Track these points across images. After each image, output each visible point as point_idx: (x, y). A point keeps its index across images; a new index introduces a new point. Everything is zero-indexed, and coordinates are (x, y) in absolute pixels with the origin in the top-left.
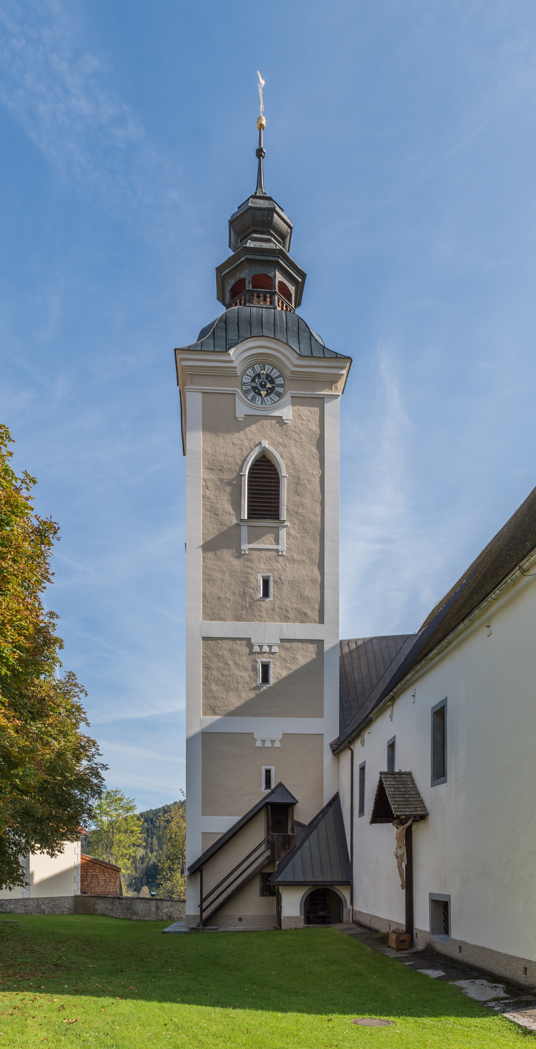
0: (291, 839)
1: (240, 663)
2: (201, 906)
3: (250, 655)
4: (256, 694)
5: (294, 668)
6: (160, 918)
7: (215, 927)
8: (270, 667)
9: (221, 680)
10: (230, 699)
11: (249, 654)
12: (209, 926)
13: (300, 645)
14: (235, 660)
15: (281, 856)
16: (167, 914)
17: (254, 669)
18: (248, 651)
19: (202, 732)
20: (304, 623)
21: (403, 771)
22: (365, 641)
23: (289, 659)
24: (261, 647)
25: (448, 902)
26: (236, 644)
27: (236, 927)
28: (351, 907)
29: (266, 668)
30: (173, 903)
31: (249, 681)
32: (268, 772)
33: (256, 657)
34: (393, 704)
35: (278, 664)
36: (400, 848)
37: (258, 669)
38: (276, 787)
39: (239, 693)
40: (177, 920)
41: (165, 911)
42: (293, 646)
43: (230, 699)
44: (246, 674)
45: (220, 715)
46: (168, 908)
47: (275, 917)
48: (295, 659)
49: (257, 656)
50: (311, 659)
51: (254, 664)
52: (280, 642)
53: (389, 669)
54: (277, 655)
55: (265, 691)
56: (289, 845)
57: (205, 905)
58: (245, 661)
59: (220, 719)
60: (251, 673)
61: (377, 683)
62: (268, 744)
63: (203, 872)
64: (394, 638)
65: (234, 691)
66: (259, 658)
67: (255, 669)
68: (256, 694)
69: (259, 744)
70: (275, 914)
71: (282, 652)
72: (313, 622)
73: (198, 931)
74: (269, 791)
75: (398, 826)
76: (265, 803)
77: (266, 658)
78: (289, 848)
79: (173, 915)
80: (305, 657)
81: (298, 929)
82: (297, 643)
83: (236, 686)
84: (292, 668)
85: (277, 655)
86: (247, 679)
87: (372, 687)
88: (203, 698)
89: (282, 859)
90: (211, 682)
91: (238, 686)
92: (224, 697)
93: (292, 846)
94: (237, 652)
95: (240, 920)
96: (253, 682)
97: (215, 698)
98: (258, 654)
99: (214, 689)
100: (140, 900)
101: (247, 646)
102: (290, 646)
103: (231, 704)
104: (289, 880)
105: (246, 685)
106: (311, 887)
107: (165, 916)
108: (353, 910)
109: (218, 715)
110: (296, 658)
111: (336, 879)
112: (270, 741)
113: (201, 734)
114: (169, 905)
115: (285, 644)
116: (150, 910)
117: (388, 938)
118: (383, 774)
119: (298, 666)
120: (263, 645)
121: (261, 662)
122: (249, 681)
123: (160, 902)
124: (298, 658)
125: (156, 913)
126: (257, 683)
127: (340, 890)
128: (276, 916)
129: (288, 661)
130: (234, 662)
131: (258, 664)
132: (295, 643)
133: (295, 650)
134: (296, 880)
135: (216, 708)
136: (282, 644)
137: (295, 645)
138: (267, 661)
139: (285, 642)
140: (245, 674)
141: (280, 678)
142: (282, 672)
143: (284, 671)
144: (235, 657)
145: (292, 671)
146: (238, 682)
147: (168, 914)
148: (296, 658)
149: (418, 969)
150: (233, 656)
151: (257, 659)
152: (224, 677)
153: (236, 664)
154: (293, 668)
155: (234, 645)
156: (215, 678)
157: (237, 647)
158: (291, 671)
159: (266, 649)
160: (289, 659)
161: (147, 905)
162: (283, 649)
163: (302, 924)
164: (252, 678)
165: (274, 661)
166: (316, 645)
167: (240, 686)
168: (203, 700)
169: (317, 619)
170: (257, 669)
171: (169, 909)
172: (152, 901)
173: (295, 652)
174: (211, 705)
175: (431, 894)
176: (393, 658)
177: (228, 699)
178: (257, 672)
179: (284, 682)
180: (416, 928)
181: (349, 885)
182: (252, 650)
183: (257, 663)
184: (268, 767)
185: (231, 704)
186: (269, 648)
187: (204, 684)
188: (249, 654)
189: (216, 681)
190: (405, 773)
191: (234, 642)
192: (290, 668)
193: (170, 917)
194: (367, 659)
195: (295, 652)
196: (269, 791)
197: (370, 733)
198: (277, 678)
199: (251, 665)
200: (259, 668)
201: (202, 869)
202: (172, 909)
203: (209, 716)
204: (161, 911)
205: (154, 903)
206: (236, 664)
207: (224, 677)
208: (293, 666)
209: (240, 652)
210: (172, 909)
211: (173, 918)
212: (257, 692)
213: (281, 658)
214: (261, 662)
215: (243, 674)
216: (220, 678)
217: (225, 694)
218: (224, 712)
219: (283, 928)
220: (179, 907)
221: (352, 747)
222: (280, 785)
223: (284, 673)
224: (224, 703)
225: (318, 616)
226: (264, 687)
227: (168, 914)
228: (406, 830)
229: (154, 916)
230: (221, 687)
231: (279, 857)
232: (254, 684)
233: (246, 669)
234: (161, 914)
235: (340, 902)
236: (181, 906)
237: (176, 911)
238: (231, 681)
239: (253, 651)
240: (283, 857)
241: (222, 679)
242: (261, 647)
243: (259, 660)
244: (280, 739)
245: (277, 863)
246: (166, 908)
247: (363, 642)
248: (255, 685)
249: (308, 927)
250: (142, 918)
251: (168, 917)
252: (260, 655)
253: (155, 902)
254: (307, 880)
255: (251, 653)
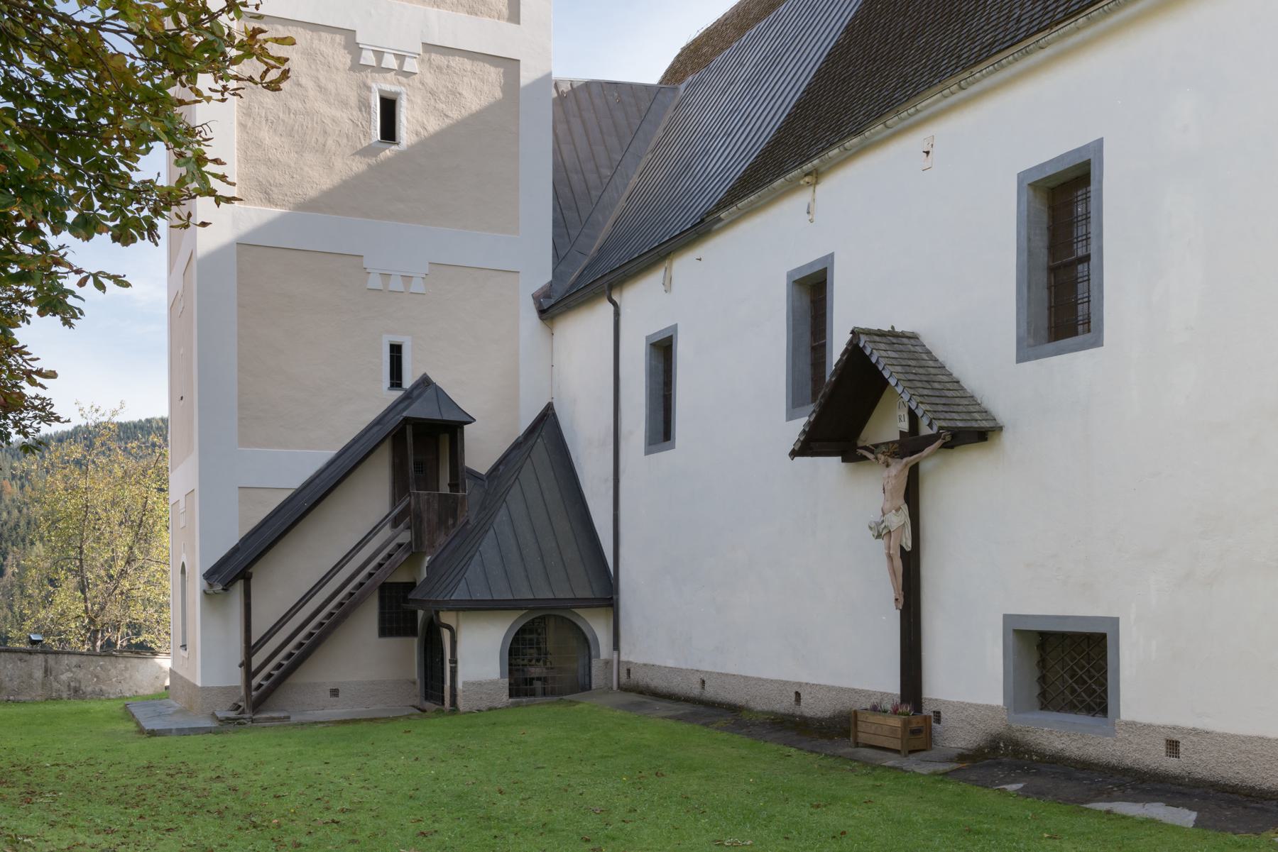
0: (459, 505)
1: (331, 86)
2: (246, 664)
3: (354, 72)
4: (369, 165)
5: (455, 115)
6: (54, 694)
7: (282, 715)
8: (401, 106)
9: (283, 121)
10: (306, 169)
11: (350, 69)
12: (272, 710)
13: (467, 64)
14: (318, 79)
15: (437, 544)
16: (69, 686)
17: (364, 105)
18: (348, 60)
19: (237, 243)
20: (476, 14)
21: (898, 329)
22: (575, 86)
23: (442, 92)
24: (379, 54)
25: (1104, 636)
26: (320, 40)
27: (326, 711)
28: (615, 656)
29: (389, 107)
30: (84, 658)
31: (350, 131)
32: (396, 350)
33: (367, 77)
34: (817, 183)
35: (419, 101)
36: (897, 510)
37: (373, 106)
38: (416, 386)
39: (328, 158)
40: (92, 698)
41: (64, 677)
42: (452, 64)
43: (306, 169)
44: (344, 115)
45: (282, 206)
46: (72, 672)
47: (414, 683)
48: (455, 94)
49: (369, 76)
50: (492, 100)
51: (365, 93)
52: (424, 52)
53: (631, 149)
54: (416, 81)
55: (389, 161)
56: (455, 518)
57: (256, 661)
58: (343, 83)
59: (283, 216)
60: (356, 113)
61: (612, 176)
62: (396, 284)
63: (253, 581)
64: (632, 87)
65: (317, 151)
66: (374, 80)
67: (364, 105)
68: (369, 165)
69: (375, 282)
70: (416, 677)
71: (429, 75)
72: (496, 15)
73: (239, 724)
74: (397, 394)
75: (890, 460)
76: (401, 419)
77: (390, 84)
78: (454, 525)
79: (83, 688)
80: (479, 93)
81: (496, 709)
82: (461, 59)
83: (321, 140)
84: (450, 114)
85: (416, 81)
86: (347, 127)
87: (602, 184)
88: (239, 161)
89: (439, 551)
90: (260, 122)
91: (327, 139)
92: (293, 165)
93: (461, 520)
94: (323, 59)
95: (335, 693)
96: (362, 136)
97: (269, 163)
98: (371, 72)
99: (267, 141)
100: (7, 654)
101: (345, 48)
102: (446, 63)
103: (309, 182)
104: (478, 596)
105: (345, 141)
106: (524, 612)
107: (64, 689)
108: (619, 662)
109: (276, 205)
110: (459, 94)
111: (580, 594)
112: (400, 278)
113: (235, 246)
114: (74, 664)
115: (433, 56)
116: (31, 676)
117: (856, 725)
118: (863, 333)
119: (465, 113)
120: (383, 52)
121: (380, 91)
122: (350, 131)
123: (54, 656)
124: (464, 93)
125: (43, 684)
126: (370, 139)
127: (584, 617)
128: (418, 682)
129: (442, 97)
130: (315, 82)
131: (372, 95)
132: (457, 58)
133: (457, 74)
134: (495, 598)
135: (273, 188)
136: (426, 56)
137: (456, 62)
138: (393, 91)
139: (436, 53)
140: (343, 116)
141: (424, 133)
142: (428, 121)
143: (432, 118)
144: (318, 70)
145: (451, 122)
146: (325, 132)
147: (73, 684)
148: (459, 94)
149: (1083, 803)
150: (313, 66)
151: (369, 82)
152: (292, 115)
153: (321, 89)
154: (452, 116)
155: (316, 42)
156: (269, 114)
157: (323, 48)
158: (448, 121)
159: (391, 62)
160: (442, 92)
161: (23, 665)
162: (430, 67)
163: (504, 698)
164: (358, 125)
165: (409, 93)
166: (502, 70)
167: (330, 142)
168: (240, 166)
169: (505, 11)
170: (370, 107)
171: (74, 673)
172: (35, 657)
173: (456, 79)
174: (261, 179)
175: (1007, 618)
176: (635, 128)
177: (301, 169)
178: (369, 114)
179: (432, 145)
180: (934, 697)
181: (612, 605)
182: (359, 61)
183: (371, 92)
184: (397, 339)
185: (309, 182)
186: (399, 61)
187: (242, 126)
188: (352, 68)
189: (272, 123)
190: (902, 335)
191: (314, 34)
192: (445, 115)
193: (76, 690)
194: (583, 122)
195: (456, 79)
196: (397, 394)
197: (700, 260)
198: (417, 134)
199: (355, 93)
200: (376, 105)
201: (251, 574)
202: (80, 674)
203: (255, 205)
204: (55, 679)
205: (38, 660)
206: (321, 89)
207: (292, 115)
208: (451, 111)
209: (331, 60)
210: (80, 674)
211: (84, 693)
212: (369, 161)
213: (426, 88)
214: (380, 91)
215: (338, 114)
216: (281, 115)
217: (293, 155)
218: (291, 200)
219: (461, 709)
220: (96, 667)
221: (615, 297)
222: (425, 382)
223: (434, 125)
224: (293, 177)
225: (506, 5)
226: (387, 151)
227: (73, 684)
228: (910, 468)
229: (40, 692)
230: (283, 139)
231: (432, 545)
232: (363, 141)
233: (344, 104)
234: (55, 685)
235: (585, 643)
236: (101, 666)
237: (90, 676)
238: (309, 126)
239: (361, 63)
240: (440, 545)
241: (286, 120)
242: (379, 54)
243: (375, 87)
244: (424, 276)
245: (428, 558)
246: (67, 671)
247: (570, 88)
248: (365, 144)
249: (517, 705)
250: (11, 698)
251: (72, 692)
252: (377, 75)
253: (41, 657)
254: (519, 598)
255: (357, 67)
